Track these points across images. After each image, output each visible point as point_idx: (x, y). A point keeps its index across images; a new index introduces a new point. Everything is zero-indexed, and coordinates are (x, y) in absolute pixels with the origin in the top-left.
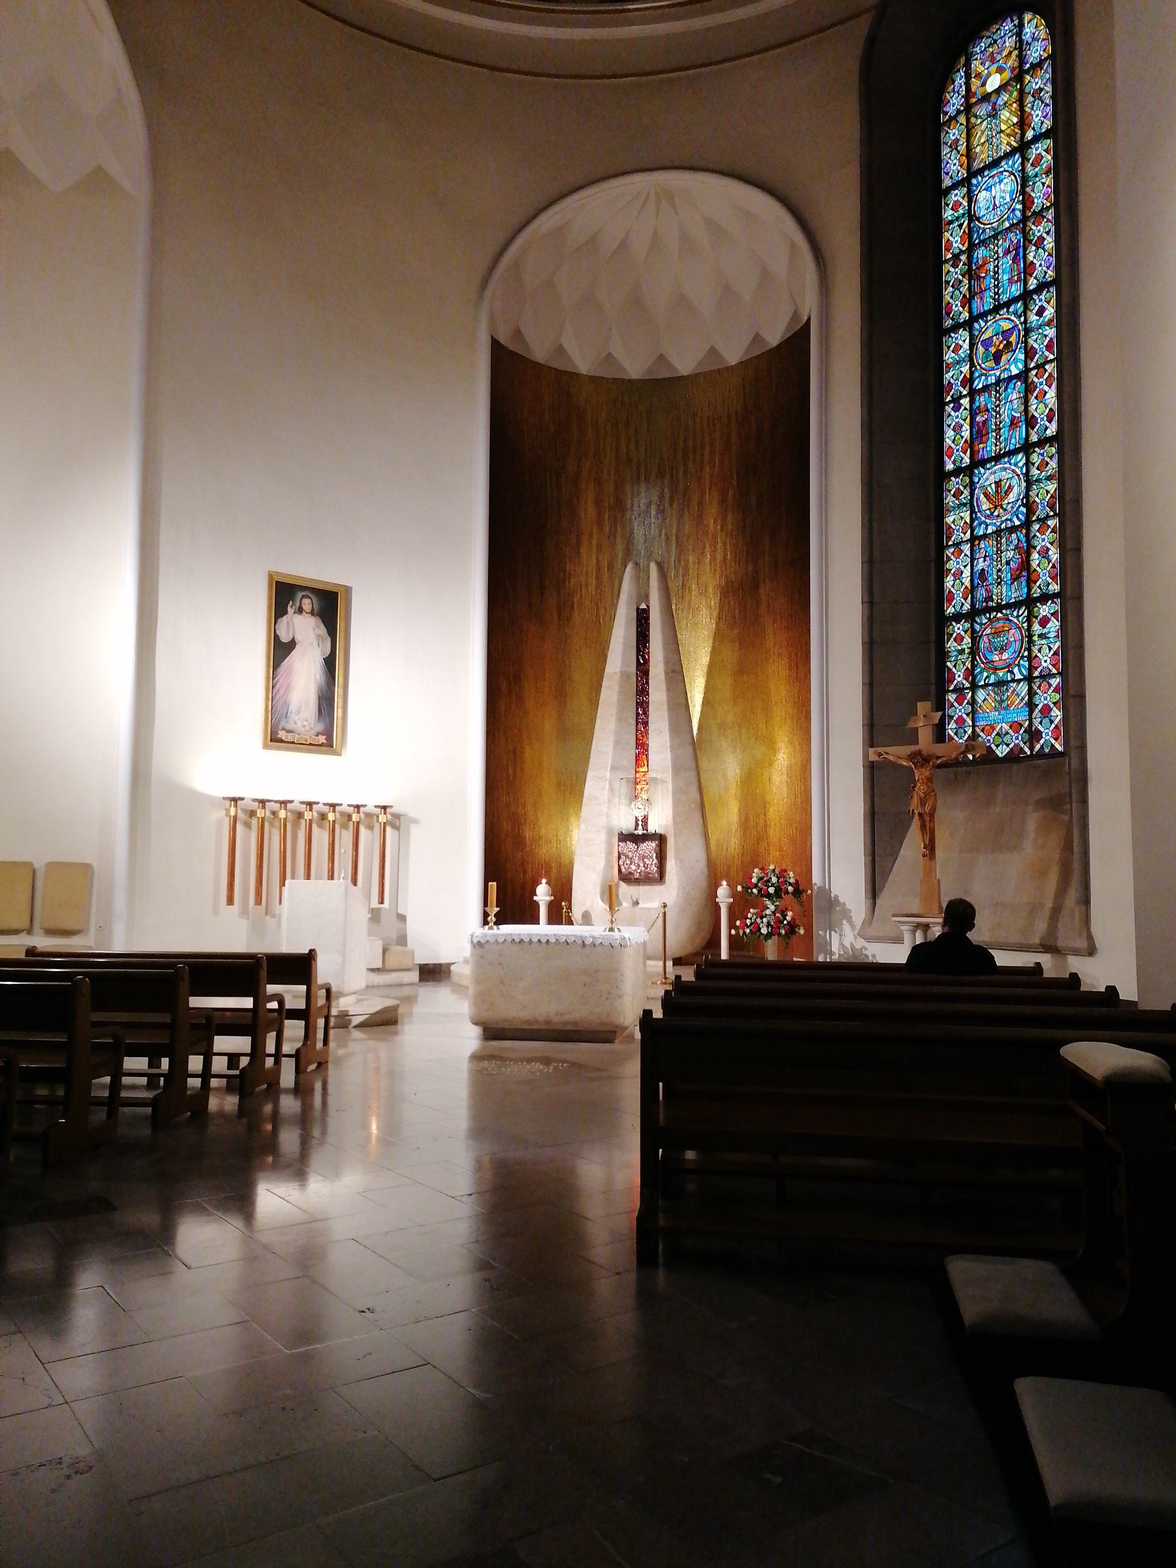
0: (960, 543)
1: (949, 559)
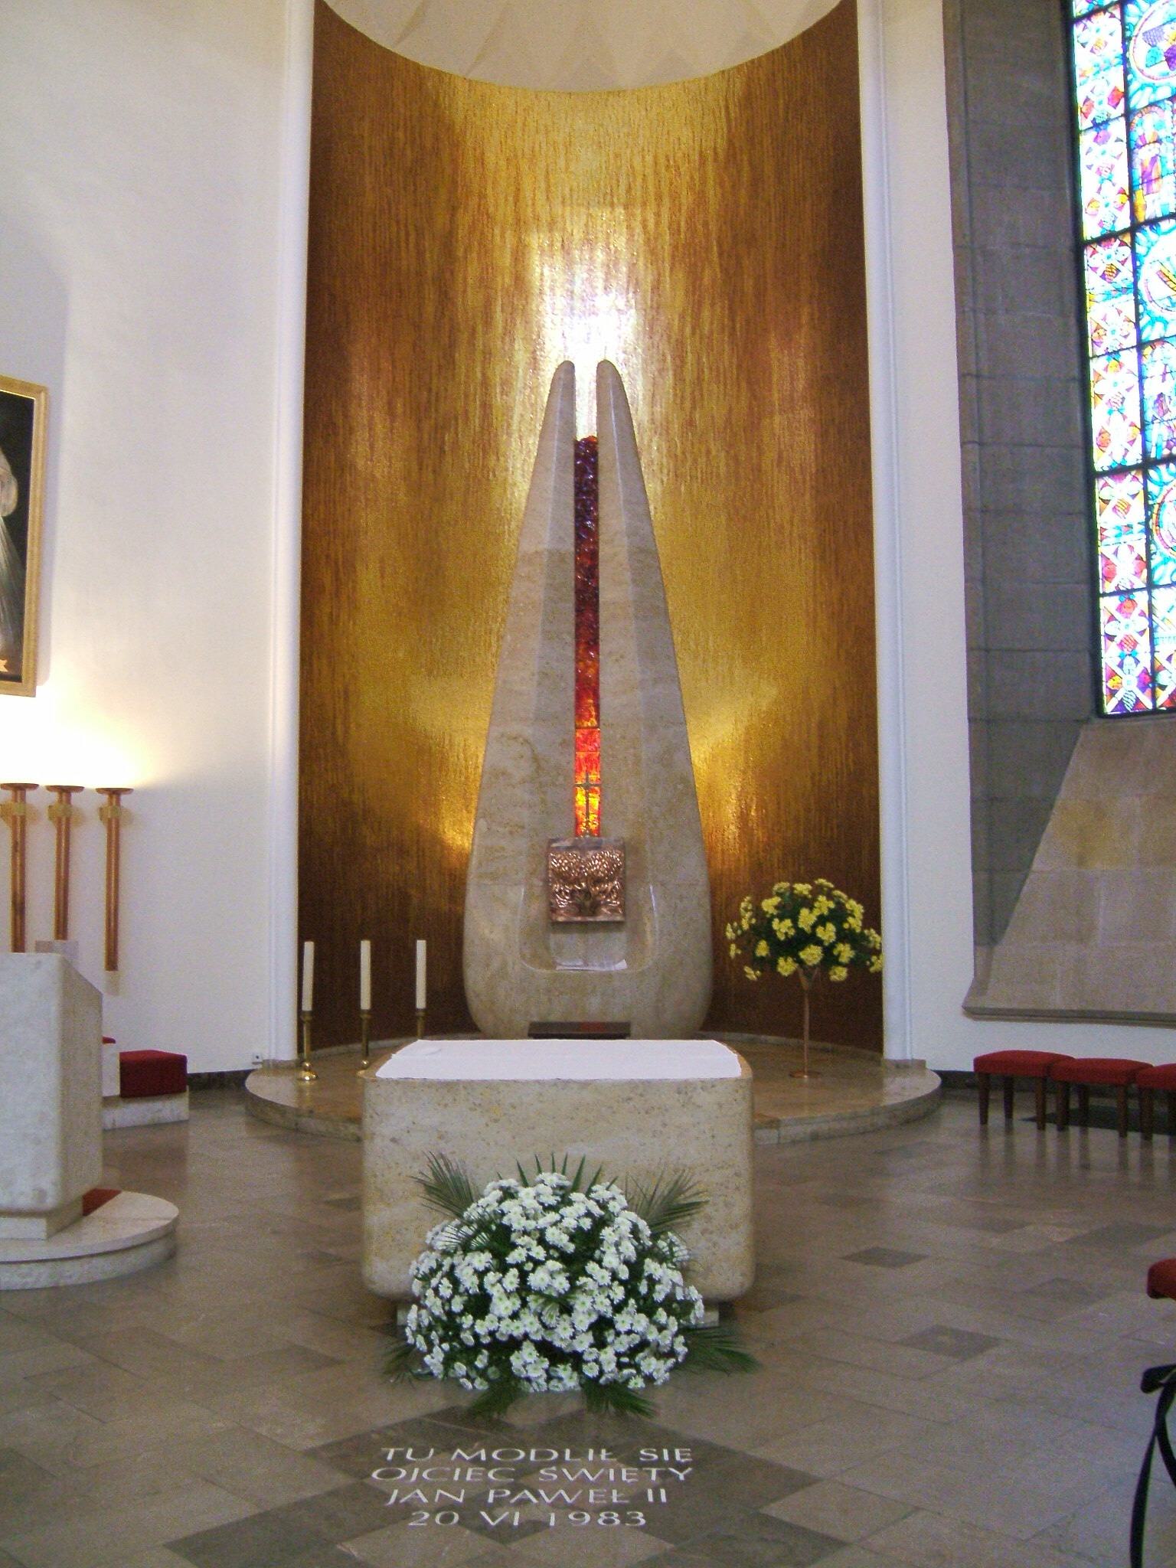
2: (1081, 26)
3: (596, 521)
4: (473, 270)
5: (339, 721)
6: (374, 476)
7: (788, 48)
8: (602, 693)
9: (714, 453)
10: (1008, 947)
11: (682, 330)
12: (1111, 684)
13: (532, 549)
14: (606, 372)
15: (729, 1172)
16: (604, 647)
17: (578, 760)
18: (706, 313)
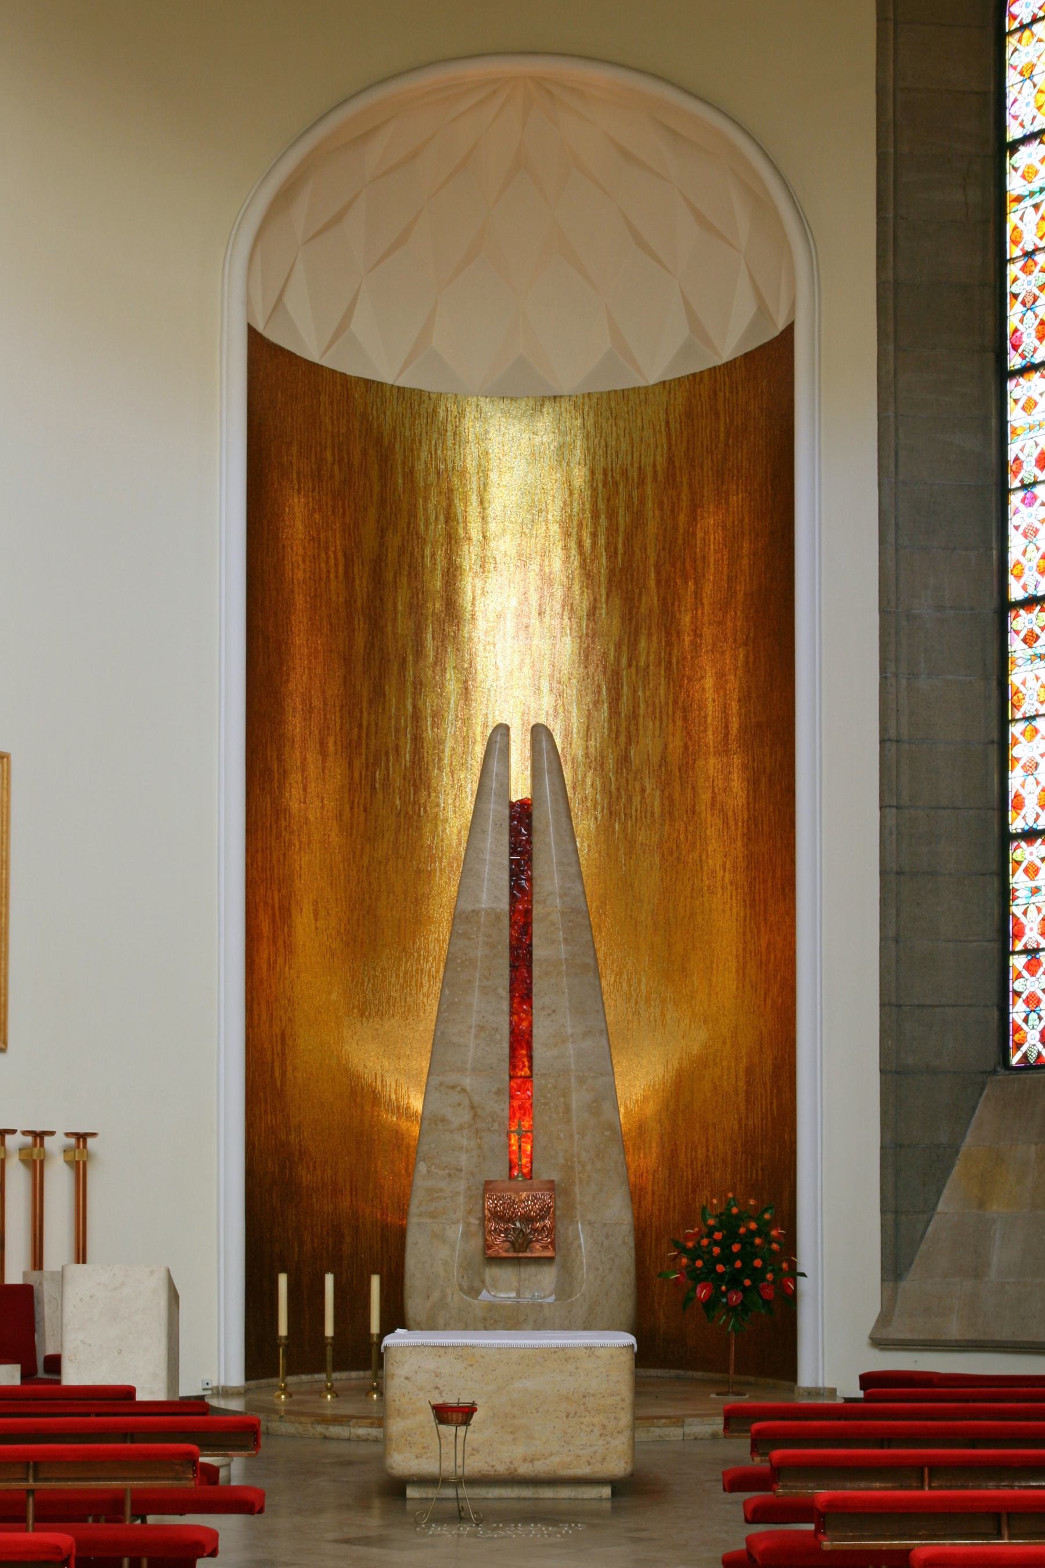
0: (1033, 718)
1: (1016, 742)
2: (1014, 382)
3: (530, 880)
4: (402, 598)
5: (277, 1064)
6: (307, 819)
7: (730, 365)
8: (536, 1045)
9: (648, 791)
10: (910, 1283)
11: (618, 660)
12: (1017, 1037)
13: (470, 908)
14: (539, 733)
15: (618, 1398)
16: (537, 1002)
17: (511, 1107)
18: (643, 644)
